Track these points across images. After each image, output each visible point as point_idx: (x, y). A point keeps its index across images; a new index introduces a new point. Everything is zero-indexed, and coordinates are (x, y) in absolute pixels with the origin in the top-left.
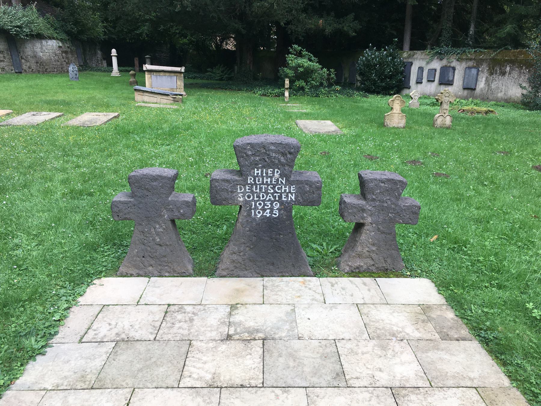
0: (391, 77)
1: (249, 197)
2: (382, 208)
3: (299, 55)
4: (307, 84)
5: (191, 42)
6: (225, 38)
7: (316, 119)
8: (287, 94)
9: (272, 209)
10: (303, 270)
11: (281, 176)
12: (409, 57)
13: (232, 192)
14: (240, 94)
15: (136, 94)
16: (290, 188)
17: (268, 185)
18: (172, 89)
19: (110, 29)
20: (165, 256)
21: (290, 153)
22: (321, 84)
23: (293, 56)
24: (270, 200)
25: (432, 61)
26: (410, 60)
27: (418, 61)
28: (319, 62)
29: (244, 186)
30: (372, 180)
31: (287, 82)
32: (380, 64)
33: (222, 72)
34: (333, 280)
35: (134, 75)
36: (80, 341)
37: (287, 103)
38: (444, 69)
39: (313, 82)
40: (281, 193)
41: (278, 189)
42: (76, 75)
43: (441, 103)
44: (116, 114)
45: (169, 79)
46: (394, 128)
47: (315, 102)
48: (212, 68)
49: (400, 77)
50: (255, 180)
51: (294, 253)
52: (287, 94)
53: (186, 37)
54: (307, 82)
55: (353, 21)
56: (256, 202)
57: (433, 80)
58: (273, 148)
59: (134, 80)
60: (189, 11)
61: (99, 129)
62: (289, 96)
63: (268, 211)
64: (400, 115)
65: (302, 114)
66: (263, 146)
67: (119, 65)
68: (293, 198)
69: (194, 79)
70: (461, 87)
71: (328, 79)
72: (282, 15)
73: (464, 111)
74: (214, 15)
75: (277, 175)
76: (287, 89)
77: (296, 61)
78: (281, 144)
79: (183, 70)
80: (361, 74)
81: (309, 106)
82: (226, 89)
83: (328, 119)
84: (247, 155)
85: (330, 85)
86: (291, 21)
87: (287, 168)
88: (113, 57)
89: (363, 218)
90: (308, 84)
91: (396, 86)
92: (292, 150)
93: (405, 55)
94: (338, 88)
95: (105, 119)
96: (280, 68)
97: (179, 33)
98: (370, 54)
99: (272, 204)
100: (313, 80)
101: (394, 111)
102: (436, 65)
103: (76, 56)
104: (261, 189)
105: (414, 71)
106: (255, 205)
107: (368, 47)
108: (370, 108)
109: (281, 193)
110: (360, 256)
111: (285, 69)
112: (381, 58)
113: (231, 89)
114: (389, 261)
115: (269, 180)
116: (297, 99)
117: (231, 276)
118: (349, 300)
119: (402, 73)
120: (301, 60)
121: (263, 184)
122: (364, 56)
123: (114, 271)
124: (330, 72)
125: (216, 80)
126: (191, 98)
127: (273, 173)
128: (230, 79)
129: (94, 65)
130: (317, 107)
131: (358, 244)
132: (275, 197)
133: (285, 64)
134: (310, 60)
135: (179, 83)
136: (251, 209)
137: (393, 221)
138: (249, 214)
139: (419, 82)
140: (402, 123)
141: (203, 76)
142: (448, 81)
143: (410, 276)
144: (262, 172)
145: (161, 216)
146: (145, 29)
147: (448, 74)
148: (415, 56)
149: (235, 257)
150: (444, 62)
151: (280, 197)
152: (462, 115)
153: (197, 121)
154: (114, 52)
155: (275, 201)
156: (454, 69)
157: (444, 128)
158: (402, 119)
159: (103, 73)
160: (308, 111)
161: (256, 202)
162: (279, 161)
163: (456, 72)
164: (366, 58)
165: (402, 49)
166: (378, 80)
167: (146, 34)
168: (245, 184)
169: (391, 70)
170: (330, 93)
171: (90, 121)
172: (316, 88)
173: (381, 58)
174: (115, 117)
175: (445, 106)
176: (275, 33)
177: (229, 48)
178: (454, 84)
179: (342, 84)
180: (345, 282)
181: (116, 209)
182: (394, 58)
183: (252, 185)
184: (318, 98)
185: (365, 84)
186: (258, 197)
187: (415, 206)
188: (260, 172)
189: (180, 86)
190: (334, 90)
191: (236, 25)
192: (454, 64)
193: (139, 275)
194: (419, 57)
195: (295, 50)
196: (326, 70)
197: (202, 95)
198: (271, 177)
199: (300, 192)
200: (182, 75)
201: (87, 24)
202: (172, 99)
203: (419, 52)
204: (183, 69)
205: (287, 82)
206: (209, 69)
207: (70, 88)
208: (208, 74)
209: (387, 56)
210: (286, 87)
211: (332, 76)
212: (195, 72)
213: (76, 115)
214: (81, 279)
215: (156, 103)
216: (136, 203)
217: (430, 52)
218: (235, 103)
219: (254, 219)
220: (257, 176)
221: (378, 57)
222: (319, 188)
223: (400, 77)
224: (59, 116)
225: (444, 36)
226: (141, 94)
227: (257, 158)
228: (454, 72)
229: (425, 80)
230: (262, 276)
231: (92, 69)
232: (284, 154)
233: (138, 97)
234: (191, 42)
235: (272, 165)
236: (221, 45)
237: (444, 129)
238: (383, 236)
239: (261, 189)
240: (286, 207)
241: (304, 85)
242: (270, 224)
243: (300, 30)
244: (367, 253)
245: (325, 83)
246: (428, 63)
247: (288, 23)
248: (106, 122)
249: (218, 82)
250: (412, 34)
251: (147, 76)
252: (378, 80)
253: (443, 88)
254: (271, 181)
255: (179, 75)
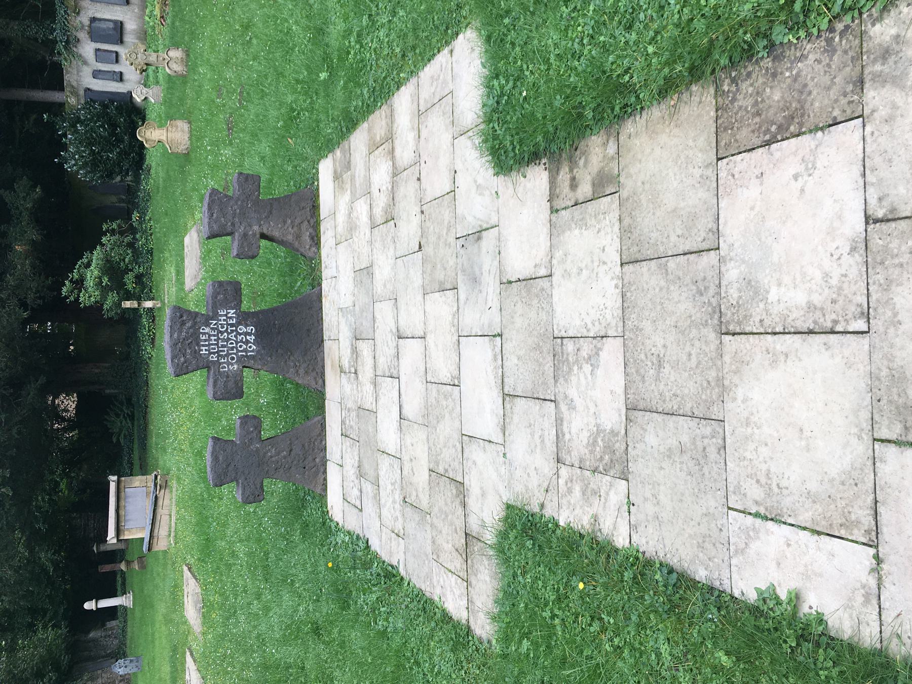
0: (114, 125)
1: (233, 359)
2: (243, 214)
3: (79, 284)
4: (131, 270)
5: (64, 474)
6: (55, 414)
7: (183, 260)
8: (148, 304)
9: (246, 334)
10: (315, 298)
11: (208, 325)
12: (74, 93)
13: (228, 377)
14: (153, 382)
15: (156, 548)
16: (221, 316)
17: (219, 339)
18: (148, 494)
19: (47, 619)
20: (303, 446)
21: (181, 316)
22: (131, 245)
23: (81, 295)
24: (236, 336)
25: (81, 56)
26: (82, 92)
27: (82, 79)
28: (92, 249)
29: (220, 364)
30: (210, 226)
31: (127, 304)
32: (90, 144)
33: (118, 416)
34: (323, 266)
35: (128, 563)
36: (361, 510)
37: (163, 302)
38: (96, 35)
39: (127, 260)
40: (228, 324)
41: (222, 327)
42: (131, 661)
43: (147, 64)
44: (185, 568)
45: (130, 500)
46: (190, 139)
47: (160, 258)
48: (112, 434)
49: (112, 110)
50: (214, 353)
51: (296, 308)
52: (148, 304)
53: (57, 484)
54: (127, 270)
55: (15, 192)
56: (238, 351)
57: (114, 55)
58: (176, 335)
59: (136, 562)
60: (11, 474)
61: (204, 586)
62: (153, 299)
63: (248, 338)
64: (170, 128)
65: (178, 280)
66: (174, 345)
67: (113, 595)
68: (232, 311)
69: (132, 464)
70: (125, 8)
71: (122, 233)
72: (9, 315)
73: (162, 17)
74: (14, 431)
75: (207, 330)
76: (139, 304)
77: (90, 289)
78: (171, 327)
79: (115, 478)
80: (110, 175)
81: (167, 267)
82: (147, 407)
83: (183, 241)
84: (185, 362)
85: (133, 230)
86: (20, 300)
87: (198, 320)
88: (100, 606)
89: (254, 235)
90: (130, 267)
91: (130, 117)
92: (178, 314)
93: (72, 101)
94: (135, 216)
95: (192, 581)
96: (105, 316)
97: (50, 495)
98: (74, 161)
99: (240, 334)
100: (124, 260)
101: (164, 138)
102: (88, 49)
103: (99, 672)
104: (223, 346)
105: (99, 85)
106: (241, 351)
107: (61, 165)
108: (165, 167)
109: (228, 324)
110: (298, 237)
111: (105, 307)
112: (80, 143)
113: (146, 398)
114: (303, 204)
115: (213, 338)
116: (158, 287)
117: (323, 375)
118: (334, 250)
119: (105, 106)
120: (90, 279)
121: (217, 344)
122: (77, 172)
123: (322, 497)
124: (107, 231)
125: (133, 424)
126: (161, 463)
127: (204, 334)
128: (129, 400)
129: (116, 642)
130: (167, 254)
131: (285, 239)
132: (232, 331)
133: (97, 308)
134: (88, 265)
135: (137, 484)
136: (246, 356)
137: (257, 202)
138: (253, 357)
139: (120, 77)
140: (183, 125)
141: (126, 449)
142: (114, 29)
143: (318, 180)
144: (203, 346)
145: (257, 450)
146: (45, 556)
147: (104, 30)
148: (75, 84)
149: (302, 371)
150: (82, 35)
151: (232, 325)
152: (169, 21)
153: (191, 444)
154: (89, 605)
155: (236, 330)
156: (93, 20)
157: (187, 62)
158: (177, 127)
159: (129, 623)
160: (173, 270)
161: (238, 351)
162: (191, 328)
163: (98, 15)
164: (80, 168)
165: (62, 105)
166: (118, 147)
167: (54, 554)
168: (218, 363)
169: (100, 126)
170: (146, 231)
171: (196, 603)
172: (136, 253)
173: (80, 143)
174: (189, 569)
175: (153, 58)
176: (43, 323)
177: (74, 406)
178: (120, 19)
179: (130, 206)
180: (324, 252)
181: (251, 498)
182: (78, 120)
183: (219, 356)
184: (154, 251)
185: (128, 170)
186: (232, 349)
187: (239, 178)
188: (204, 348)
189: (141, 481)
190: (141, 223)
191: (32, 393)
192: (84, 19)
193: (325, 472)
194: (75, 77)
195: (72, 292)
196: (104, 239)
197: (157, 444)
198: (210, 336)
199: (226, 304)
200: (123, 479)
201: (41, 656)
202: (163, 491)
203: (66, 77)
204: (113, 478)
205: (127, 304)
206: (114, 440)
207: (154, 661)
208: (122, 441)
209: (76, 131)
210: (136, 306)
211: (115, 226)
212: (121, 464)
213: (189, 631)
214: (327, 527)
215: (170, 516)
216: (243, 478)
217: (66, 59)
218: (165, 388)
219: (258, 352)
220: (209, 350)
221: (77, 147)
222: (221, 284)
223: (112, 110)
224: (192, 654)
225: (36, 33)
226: (155, 540)
227: (189, 351)
228: (100, 20)
229: (117, 68)
230: (322, 341)
231: (123, 644)
232: (183, 323)
233: (161, 545)
234: (64, 474)
235: (195, 337)
236: (69, 420)
237: (189, 58)
238: (274, 212)
239: (223, 346)
240: (244, 318)
241: (133, 274)
242: (260, 336)
243: (34, 285)
244: (295, 229)
245: (129, 239)
246: (85, 63)
247: (24, 305)
248: (196, 579)
249: (136, 423)
250: (35, 86)
251: (126, 536)
252: (118, 147)
253: (129, 38)
254: (214, 336)
255: (122, 484)
